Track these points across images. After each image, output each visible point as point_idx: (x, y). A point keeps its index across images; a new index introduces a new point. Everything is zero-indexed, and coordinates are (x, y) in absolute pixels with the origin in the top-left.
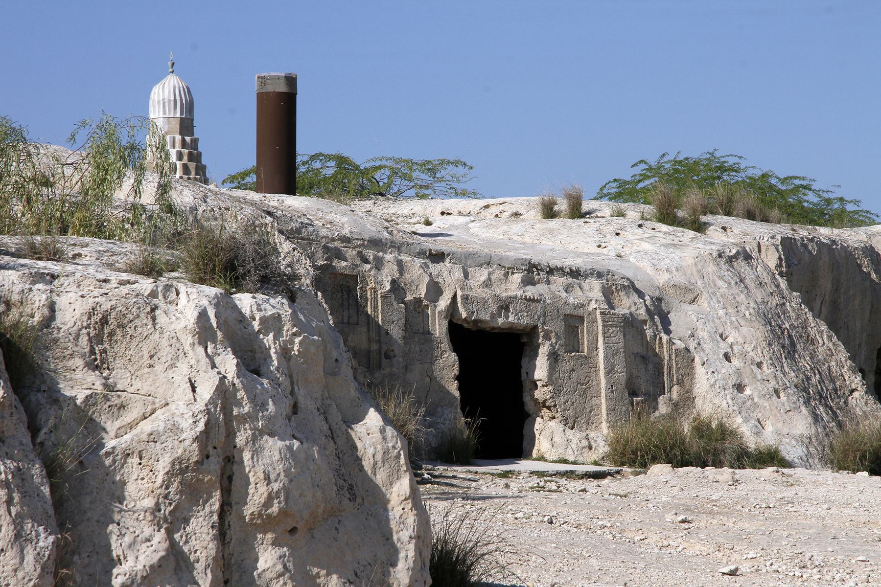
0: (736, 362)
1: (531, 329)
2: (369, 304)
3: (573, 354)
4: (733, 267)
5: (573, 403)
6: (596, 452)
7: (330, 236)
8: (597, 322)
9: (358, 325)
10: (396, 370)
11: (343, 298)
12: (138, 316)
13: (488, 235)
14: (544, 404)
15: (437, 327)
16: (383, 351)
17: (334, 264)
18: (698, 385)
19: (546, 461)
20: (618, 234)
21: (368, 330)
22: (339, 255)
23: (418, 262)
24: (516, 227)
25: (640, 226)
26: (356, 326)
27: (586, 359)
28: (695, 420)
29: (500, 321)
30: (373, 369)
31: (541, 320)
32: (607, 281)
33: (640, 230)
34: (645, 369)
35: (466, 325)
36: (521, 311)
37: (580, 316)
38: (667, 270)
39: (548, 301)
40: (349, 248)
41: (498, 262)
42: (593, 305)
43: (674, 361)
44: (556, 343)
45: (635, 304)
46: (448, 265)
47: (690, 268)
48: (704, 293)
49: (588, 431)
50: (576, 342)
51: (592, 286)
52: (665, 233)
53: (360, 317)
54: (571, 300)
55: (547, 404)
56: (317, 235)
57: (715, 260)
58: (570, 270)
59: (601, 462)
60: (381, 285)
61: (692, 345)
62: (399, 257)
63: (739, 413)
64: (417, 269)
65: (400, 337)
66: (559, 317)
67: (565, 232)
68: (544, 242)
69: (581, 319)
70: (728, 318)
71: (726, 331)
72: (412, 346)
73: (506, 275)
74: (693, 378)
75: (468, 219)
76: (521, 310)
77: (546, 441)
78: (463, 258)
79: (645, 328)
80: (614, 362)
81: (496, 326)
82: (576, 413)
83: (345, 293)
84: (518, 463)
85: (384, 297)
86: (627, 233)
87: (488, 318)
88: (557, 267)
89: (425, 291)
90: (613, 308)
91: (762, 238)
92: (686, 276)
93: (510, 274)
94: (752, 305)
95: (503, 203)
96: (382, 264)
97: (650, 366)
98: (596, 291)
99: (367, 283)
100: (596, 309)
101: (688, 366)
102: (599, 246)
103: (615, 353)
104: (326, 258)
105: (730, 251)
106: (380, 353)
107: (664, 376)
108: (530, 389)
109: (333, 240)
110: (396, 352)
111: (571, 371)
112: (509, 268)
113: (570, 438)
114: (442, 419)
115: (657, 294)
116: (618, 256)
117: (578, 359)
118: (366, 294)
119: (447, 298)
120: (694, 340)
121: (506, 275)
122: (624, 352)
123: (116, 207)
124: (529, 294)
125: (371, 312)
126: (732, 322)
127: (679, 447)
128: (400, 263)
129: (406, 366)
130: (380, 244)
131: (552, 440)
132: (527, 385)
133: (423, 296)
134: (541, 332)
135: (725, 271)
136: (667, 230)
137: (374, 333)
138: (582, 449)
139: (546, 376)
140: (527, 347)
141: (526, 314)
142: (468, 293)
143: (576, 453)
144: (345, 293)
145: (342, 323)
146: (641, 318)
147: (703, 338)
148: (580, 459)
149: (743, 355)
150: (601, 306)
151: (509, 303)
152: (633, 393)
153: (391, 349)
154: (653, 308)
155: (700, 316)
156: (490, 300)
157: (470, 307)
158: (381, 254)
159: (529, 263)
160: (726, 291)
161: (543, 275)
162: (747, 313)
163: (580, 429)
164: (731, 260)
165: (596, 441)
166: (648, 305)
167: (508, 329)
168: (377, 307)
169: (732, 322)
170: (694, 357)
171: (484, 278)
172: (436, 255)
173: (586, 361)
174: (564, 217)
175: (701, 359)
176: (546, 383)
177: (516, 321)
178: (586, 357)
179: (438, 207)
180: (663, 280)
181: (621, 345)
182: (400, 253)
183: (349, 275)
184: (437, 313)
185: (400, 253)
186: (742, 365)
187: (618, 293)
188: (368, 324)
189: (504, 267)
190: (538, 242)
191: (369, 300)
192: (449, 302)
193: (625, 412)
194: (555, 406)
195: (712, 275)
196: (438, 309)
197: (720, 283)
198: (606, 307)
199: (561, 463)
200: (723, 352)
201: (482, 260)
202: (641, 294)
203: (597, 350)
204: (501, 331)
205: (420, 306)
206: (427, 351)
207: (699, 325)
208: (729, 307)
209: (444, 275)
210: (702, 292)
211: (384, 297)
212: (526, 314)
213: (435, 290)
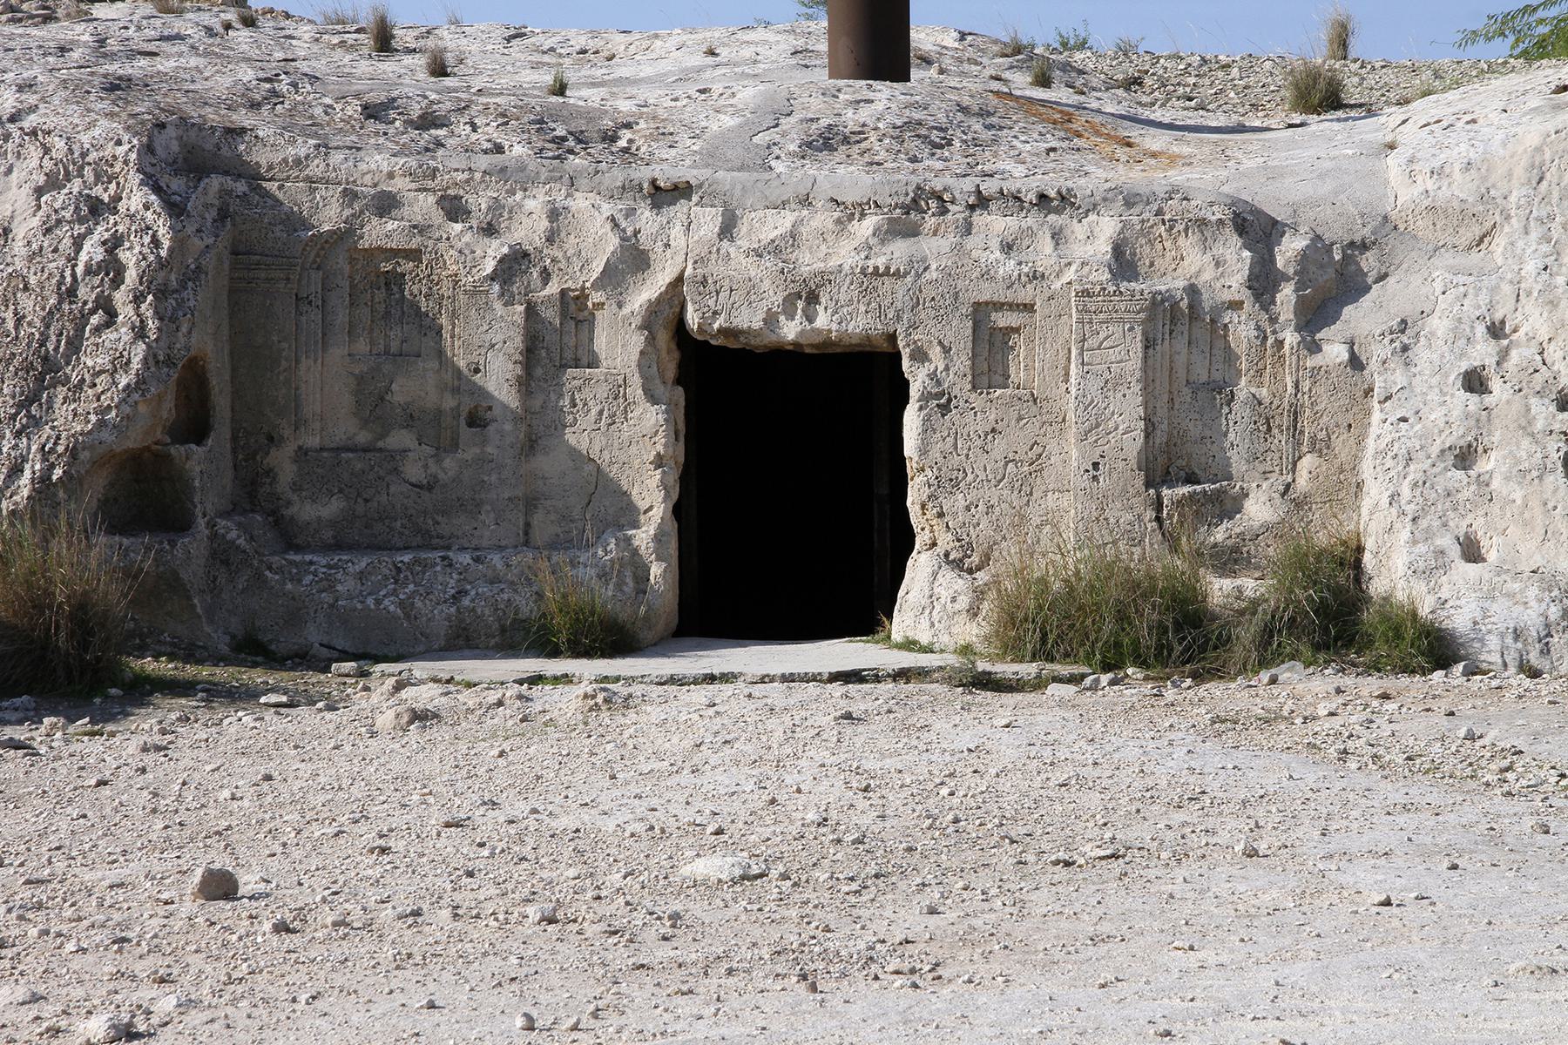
10: (495, 452)
29: (791, 330)
65: (510, 377)
72: (552, 395)
87: (757, 324)
93: (857, 216)
111: (986, 434)
123: (119, 603)
137: (450, 373)
153: (484, 405)
170: (1373, 383)
196: (626, 310)
213: (633, 259)
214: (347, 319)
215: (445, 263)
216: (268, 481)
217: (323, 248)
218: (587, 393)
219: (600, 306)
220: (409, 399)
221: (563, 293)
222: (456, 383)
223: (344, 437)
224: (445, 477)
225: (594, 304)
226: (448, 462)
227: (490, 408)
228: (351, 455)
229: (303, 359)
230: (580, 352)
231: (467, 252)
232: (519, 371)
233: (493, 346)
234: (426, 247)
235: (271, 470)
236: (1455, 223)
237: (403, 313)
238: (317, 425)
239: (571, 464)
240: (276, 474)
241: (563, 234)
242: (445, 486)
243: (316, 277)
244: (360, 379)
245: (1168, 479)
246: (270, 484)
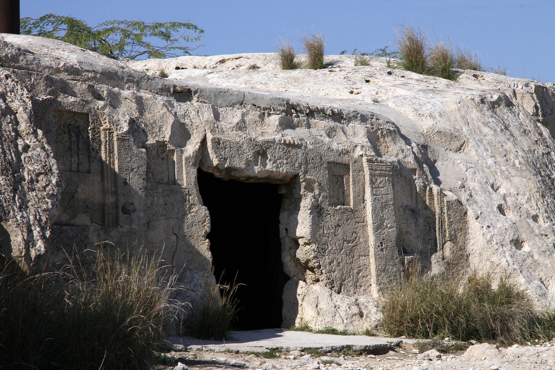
0: (511, 215)
1: (291, 179)
2: (103, 148)
3: (338, 207)
4: (496, 113)
5: (339, 263)
6: (368, 320)
7: (55, 67)
8: (363, 171)
9: (90, 173)
11: (71, 141)
13: (228, 84)
14: (305, 267)
15: (184, 176)
16: (121, 204)
17: (59, 99)
18: (472, 242)
19: (311, 331)
20: (367, 81)
21: (102, 180)
22: (66, 89)
23: (161, 99)
24: (256, 77)
25: (390, 73)
26: (87, 175)
27: (353, 213)
28: (470, 280)
29: (257, 169)
30: (108, 226)
31: (303, 169)
32: (372, 125)
33: (390, 78)
34: (416, 224)
35: (217, 174)
36: (280, 158)
37: (345, 164)
38: (431, 116)
39: (310, 147)
40: (79, 80)
41: (253, 102)
42: (358, 152)
43: (446, 215)
44: (319, 195)
45: (403, 151)
46: (195, 104)
47: (454, 113)
48: (470, 140)
49: (357, 294)
50: (341, 194)
51: (356, 130)
52: (418, 80)
53: (92, 163)
54: (335, 146)
55: (311, 264)
56: (38, 65)
57: (477, 105)
58: (333, 112)
59: (375, 332)
60: (118, 125)
61: (464, 198)
62: (139, 93)
63: (521, 272)
64: (160, 108)
66: (322, 165)
67: (311, 79)
68: (291, 90)
69: (346, 167)
70: (498, 167)
71: (497, 182)
72: (155, 198)
73: (262, 117)
74: (466, 234)
75: (205, 71)
76: (280, 157)
77: (310, 308)
78: (212, 96)
79: (414, 177)
80: (383, 216)
81: (252, 175)
82: (342, 274)
83: (73, 135)
84: (280, 336)
85: (121, 139)
86: (378, 80)
87: (242, 165)
88: (317, 108)
89: (170, 133)
90: (381, 156)
91: (516, 86)
92: (450, 122)
93: (266, 115)
94: (520, 153)
95: (239, 58)
96: (120, 103)
97: (421, 221)
98: (361, 135)
99: (101, 123)
100: (362, 156)
101: (461, 219)
102: (352, 92)
103: (384, 206)
104: (49, 92)
105: (492, 97)
106: (117, 207)
107: (435, 231)
108: (290, 248)
109: (58, 71)
110: (137, 205)
111: (336, 227)
112: (265, 109)
113: (337, 304)
114: (192, 285)
115: (422, 141)
116: (375, 102)
117: (343, 213)
118: (100, 136)
119: (195, 142)
120: (465, 191)
121: (262, 117)
122: (394, 204)
124: (288, 138)
125: (106, 157)
126: (502, 172)
127: (464, 313)
128: (139, 101)
129: (148, 223)
130: (115, 77)
131: (317, 306)
132: (286, 243)
133: (167, 139)
134: (303, 182)
135: (489, 118)
136: (418, 78)
137: (110, 183)
138: (352, 317)
139: (308, 232)
140: (286, 200)
141: (285, 161)
142: (220, 136)
143: (345, 321)
144: (73, 135)
145: (71, 170)
146: (409, 166)
147: (474, 189)
148: (351, 329)
149: (518, 208)
150: (368, 153)
151: (267, 149)
152: (404, 250)
153: (130, 202)
154: (420, 156)
155: (469, 165)
156: (245, 146)
157: (223, 153)
158: (116, 89)
159: (288, 103)
160: (493, 138)
161: (302, 117)
162: (517, 162)
163: (347, 293)
164: (493, 105)
165: (366, 307)
166: (416, 152)
167: (266, 178)
168: (113, 152)
169: (502, 172)
170: (467, 210)
171: (236, 120)
172: (182, 92)
173: (352, 215)
174: (305, 67)
175: (475, 212)
176: (309, 240)
177: (274, 169)
178: (352, 211)
179: (172, 63)
180: (427, 127)
181: (390, 196)
182: (139, 88)
183: (78, 113)
185: (139, 88)
186: (518, 218)
187: (384, 139)
188: (102, 172)
189: (259, 107)
190: (284, 90)
191: (103, 144)
192: (197, 147)
193: (396, 272)
194: (319, 267)
195: (477, 121)
197: (486, 130)
198: (373, 154)
199: (328, 333)
200: (496, 204)
201: (234, 99)
202: (408, 142)
203: (363, 202)
204: (257, 182)
205: (164, 151)
206: (172, 204)
207: (469, 174)
208: (497, 155)
209: (191, 115)
210: (468, 139)
211: (121, 139)
212: (285, 161)
228: (67, 227)
236: (449, 139)
245: (406, 253)
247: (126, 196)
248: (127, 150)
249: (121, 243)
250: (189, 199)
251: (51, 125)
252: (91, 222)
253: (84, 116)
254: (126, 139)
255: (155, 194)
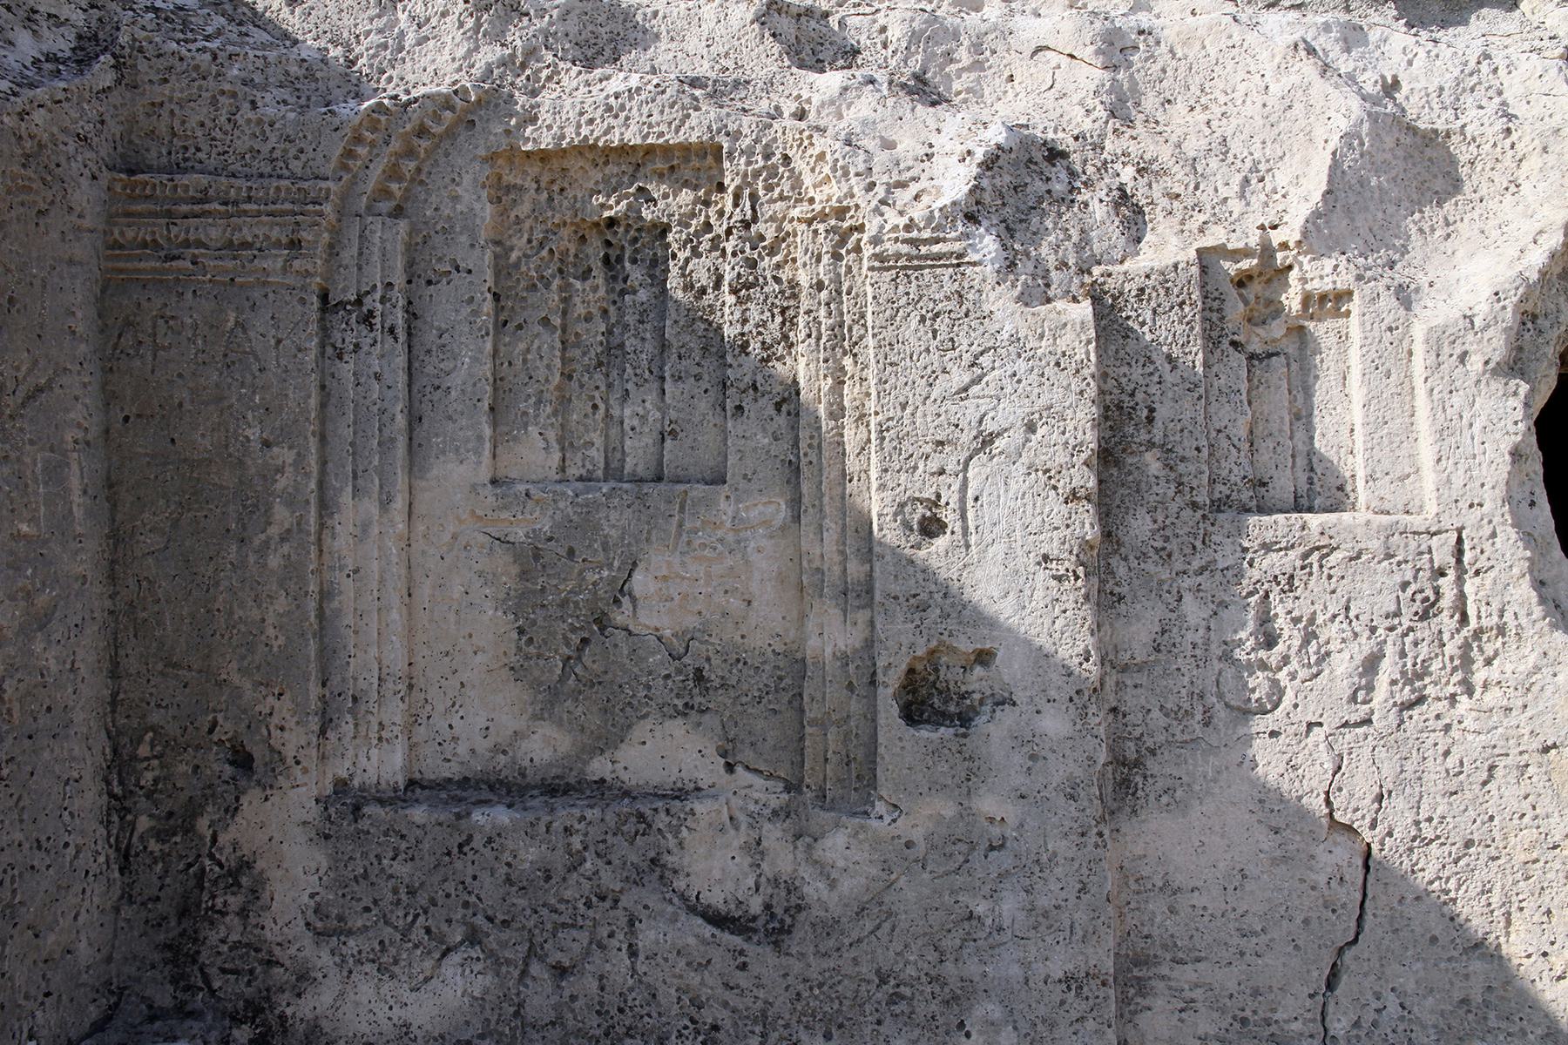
10: (1011, 812)
12: (721, 540)
65: (1053, 549)
137: (831, 537)
153: (965, 646)
184: (1419, 349)
196: (1434, 313)
214: (487, 369)
215: (797, 182)
216: (235, 902)
217: (410, 153)
218: (1315, 597)
219: (1332, 302)
220: (691, 622)
221: (1207, 259)
222: (855, 569)
223: (482, 746)
224: (832, 899)
225: (1307, 300)
226: (836, 845)
227: (984, 657)
228: (502, 816)
229: (346, 498)
230: (1265, 457)
231: (869, 143)
232: (1086, 524)
233: (987, 441)
234: (736, 136)
235: (246, 865)
237: (664, 346)
238: (394, 712)
239: (1266, 841)
240: (260, 882)
241: (1150, 102)
242: (829, 927)
243: (389, 238)
244: (531, 558)
246: (243, 913)
247: (934, 613)
248: (942, 325)
249: (890, 914)
250: (1462, 597)
251: (463, 239)
252: (730, 768)
253: (695, 163)
254: (939, 256)
255: (1187, 582)
